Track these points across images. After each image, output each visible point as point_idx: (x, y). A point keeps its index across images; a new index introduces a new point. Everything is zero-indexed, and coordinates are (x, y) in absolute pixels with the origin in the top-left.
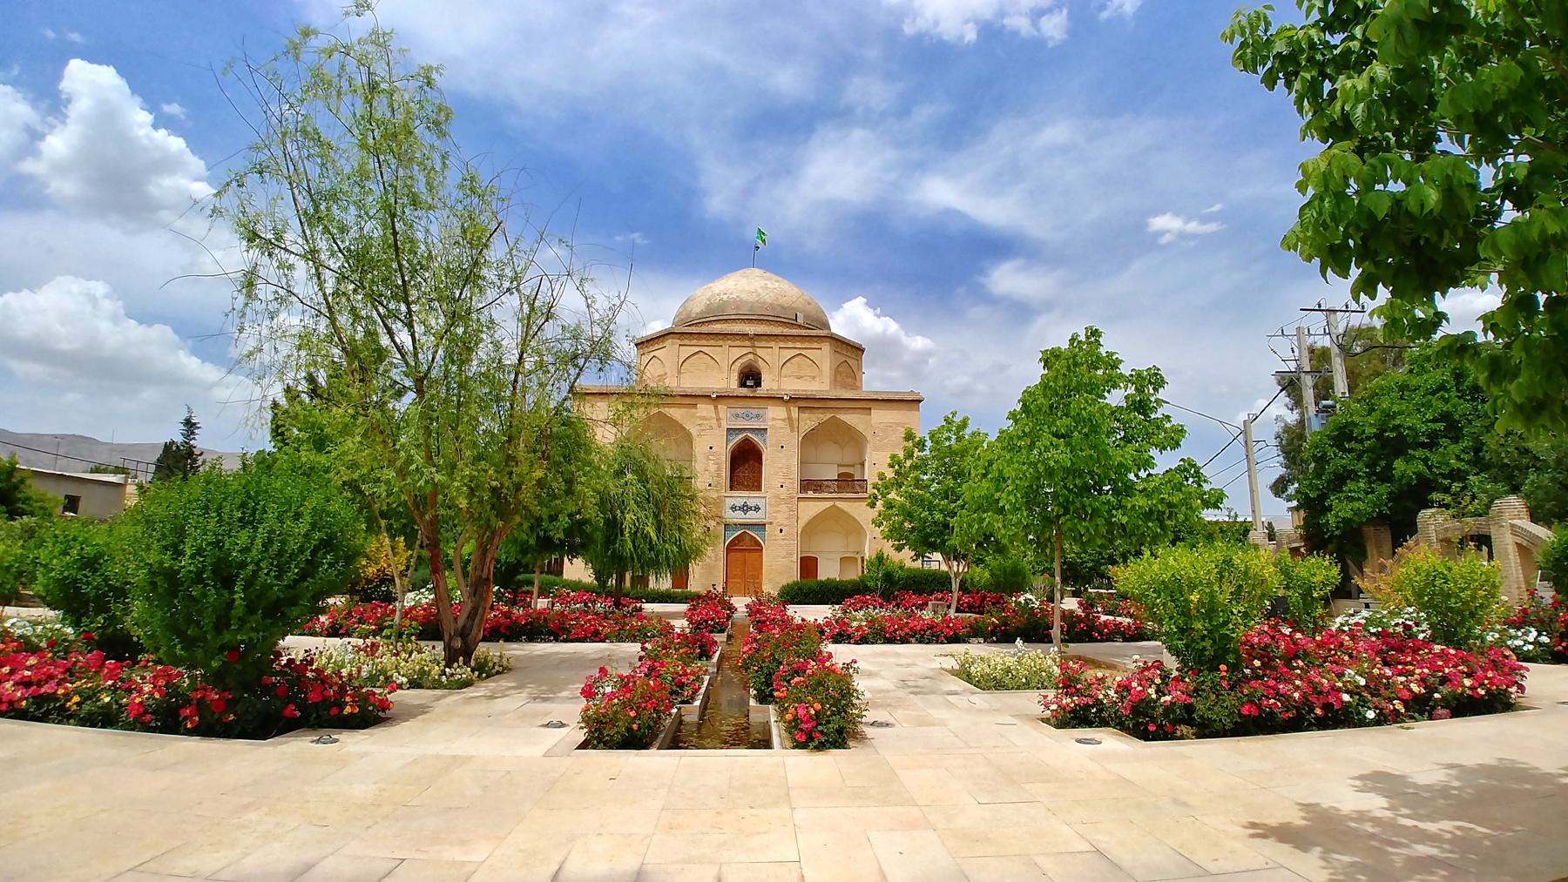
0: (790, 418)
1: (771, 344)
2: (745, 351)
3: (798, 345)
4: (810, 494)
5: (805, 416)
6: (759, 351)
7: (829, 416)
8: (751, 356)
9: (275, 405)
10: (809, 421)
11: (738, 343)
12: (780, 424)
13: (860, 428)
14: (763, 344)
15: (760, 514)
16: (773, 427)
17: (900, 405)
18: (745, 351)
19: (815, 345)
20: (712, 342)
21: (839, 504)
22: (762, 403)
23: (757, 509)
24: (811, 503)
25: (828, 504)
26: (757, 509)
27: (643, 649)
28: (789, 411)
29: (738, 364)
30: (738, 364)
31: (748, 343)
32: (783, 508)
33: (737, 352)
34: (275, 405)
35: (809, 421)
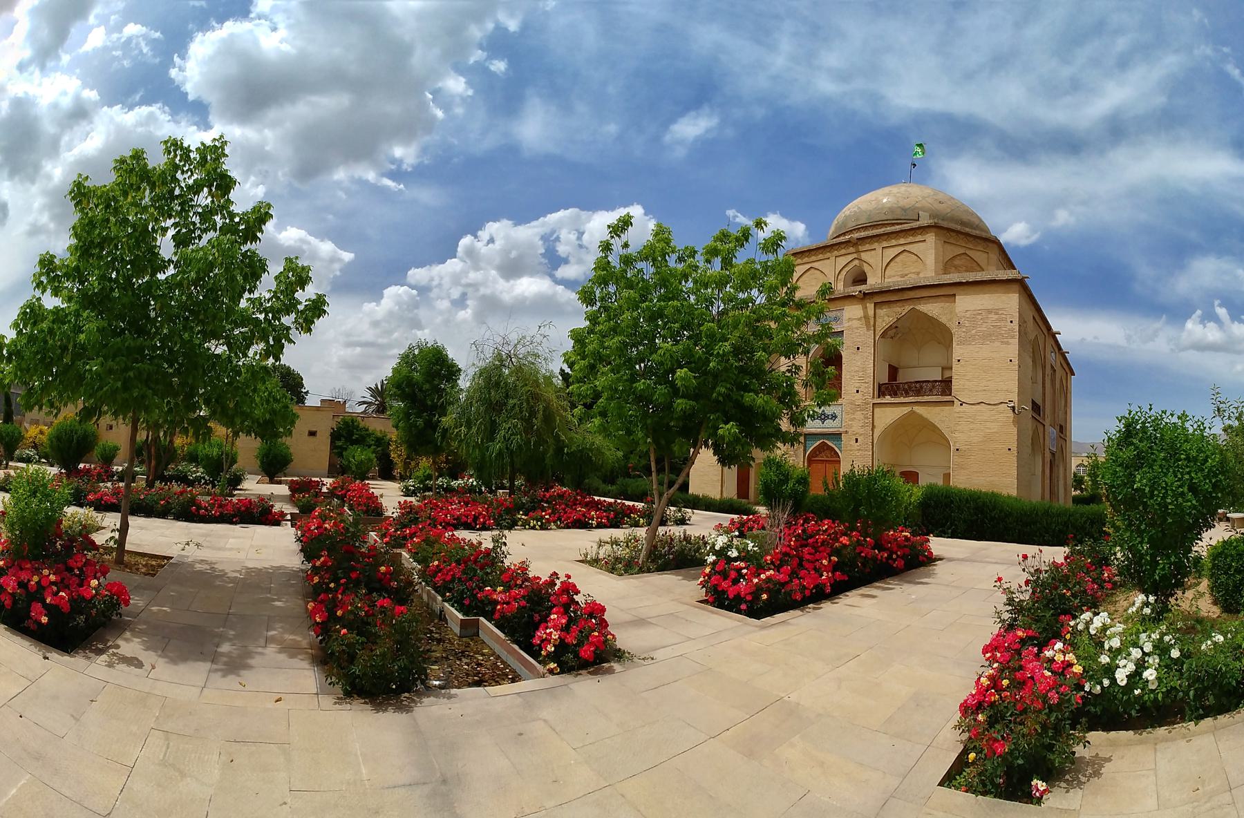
0: (866, 317)
1: (876, 245)
2: (850, 258)
3: (902, 241)
4: (888, 399)
5: (882, 312)
6: (864, 256)
7: (908, 308)
8: (856, 262)
9: (524, 337)
10: (886, 317)
11: (843, 251)
12: (856, 324)
13: (943, 320)
14: (867, 247)
15: (836, 423)
16: (850, 328)
17: (993, 287)
18: (850, 258)
19: (919, 238)
20: (821, 256)
21: (919, 410)
22: (838, 304)
23: (834, 417)
24: (888, 410)
25: (906, 410)
26: (834, 417)
27: (727, 598)
28: (865, 308)
29: (844, 273)
30: (844, 273)
31: (852, 249)
32: (859, 415)
33: (842, 261)
34: (524, 337)
35: (886, 317)
